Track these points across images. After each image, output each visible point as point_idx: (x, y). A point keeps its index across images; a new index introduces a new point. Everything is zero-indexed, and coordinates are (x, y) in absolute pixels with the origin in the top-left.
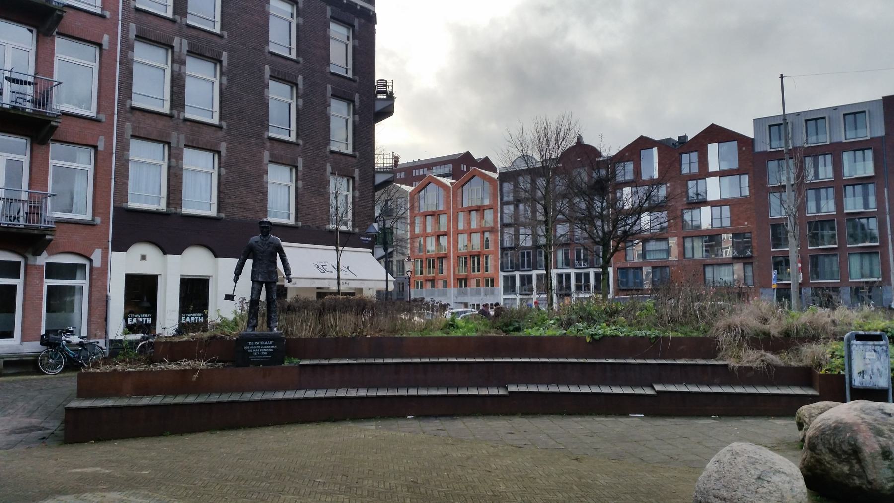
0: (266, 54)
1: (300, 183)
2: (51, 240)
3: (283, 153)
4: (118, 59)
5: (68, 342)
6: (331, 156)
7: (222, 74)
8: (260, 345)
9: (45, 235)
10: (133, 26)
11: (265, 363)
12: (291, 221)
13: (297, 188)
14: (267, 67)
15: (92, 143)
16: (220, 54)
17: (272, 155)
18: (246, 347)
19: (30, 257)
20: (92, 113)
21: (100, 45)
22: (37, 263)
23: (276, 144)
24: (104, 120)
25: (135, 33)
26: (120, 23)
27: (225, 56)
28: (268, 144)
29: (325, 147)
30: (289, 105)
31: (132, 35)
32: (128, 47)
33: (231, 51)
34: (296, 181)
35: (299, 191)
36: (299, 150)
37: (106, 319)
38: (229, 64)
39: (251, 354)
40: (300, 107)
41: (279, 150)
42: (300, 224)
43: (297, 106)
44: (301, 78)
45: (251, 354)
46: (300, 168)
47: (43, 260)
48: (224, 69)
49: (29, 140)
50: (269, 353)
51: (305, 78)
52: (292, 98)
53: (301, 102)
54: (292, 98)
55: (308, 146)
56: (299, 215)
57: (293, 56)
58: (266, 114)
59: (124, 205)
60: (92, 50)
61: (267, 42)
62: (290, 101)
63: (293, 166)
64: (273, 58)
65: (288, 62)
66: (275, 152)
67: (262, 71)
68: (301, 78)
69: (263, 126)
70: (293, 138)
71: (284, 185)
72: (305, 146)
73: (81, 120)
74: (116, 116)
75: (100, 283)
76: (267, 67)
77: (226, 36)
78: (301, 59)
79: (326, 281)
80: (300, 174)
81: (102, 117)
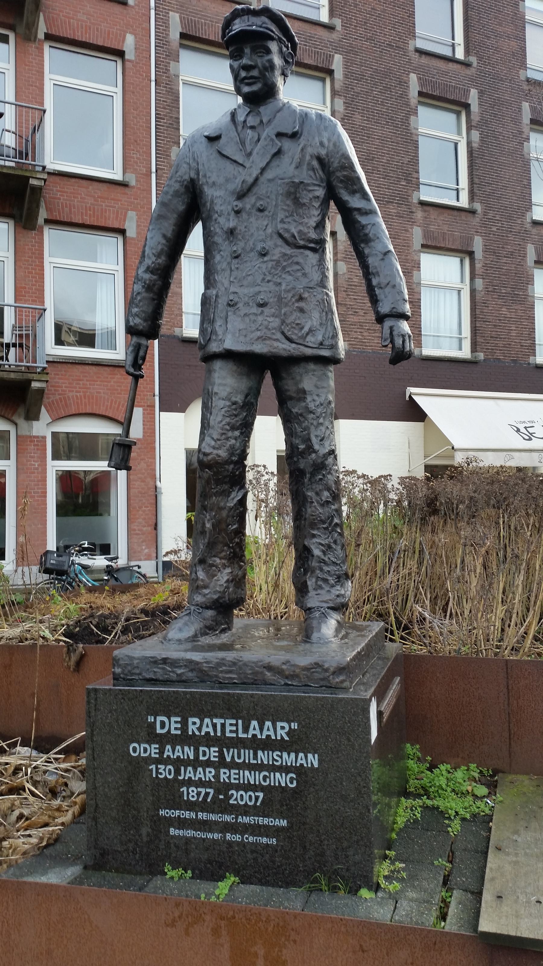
0: (411, 48)
1: (479, 283)
2: (41, 392)
3: (446, 232)
4: (153, 77)
5: (85, 567)
6: (534, 231)
7: (334, 93)
8: (222, 742)
9: (29, 382)
10: (175, 18)
11: (259, 869)
12: (465, 353)
13: (473, 292)
14: (413, 77)
15: (116, 225)
16: (330, 59)
17: (426, 234)
18: (140, 750)
19: (21, 422)
20: (117, 175)
21: (120, 54)
22: (35, 433)
23: (433, 213)
24: (133, 183)
25: (180, 30)
26: (153, 12)
27: (338, 63)
28: (419, 214)
29: (523, 215)
30: (456, 145)
31: (174, 35)
32: (168, 57)
33: (350, 53)
34: (472, 279)
35: (478, 297)
36: (476, 221)
37: (156, 527)
38: (346, 76)
39: (170, 793)
40: (475, 145)
41: (440, 223)
42: (481, 356)
43: (469, 144)
44: (474, 93)
45: (170, 793)
46: (479, 254)
47: (43, 428)
48: (337, 86)
49: (12, 223)
50: (275, 800)
51: (481, 93)
52: (459, 133)
53: (476, 135)
54: (459, 133)
55: (491, 215)
56: (479, 339)
57: (460, 54)
58: (415, 161)
59: (177, 331)
60: (111, 67)
61: (413, 35)
62: (456, 138)
63: (466, 252)
64: (424, 60)
65: (451, 65)
66: (432, 228)
67: (404, 84)
68: (474, 93)
69: (409, 182)
70: (464, 202)
71: (451, 289)
72: (485, 214)
73: (96, 184)
74: (154, 176)
75: (143, 465)
76: (413, 77)
77: (339, 27)
78: (473, 60)
79: (535, 455)
80: (478, 266)
81: (132, 179)
